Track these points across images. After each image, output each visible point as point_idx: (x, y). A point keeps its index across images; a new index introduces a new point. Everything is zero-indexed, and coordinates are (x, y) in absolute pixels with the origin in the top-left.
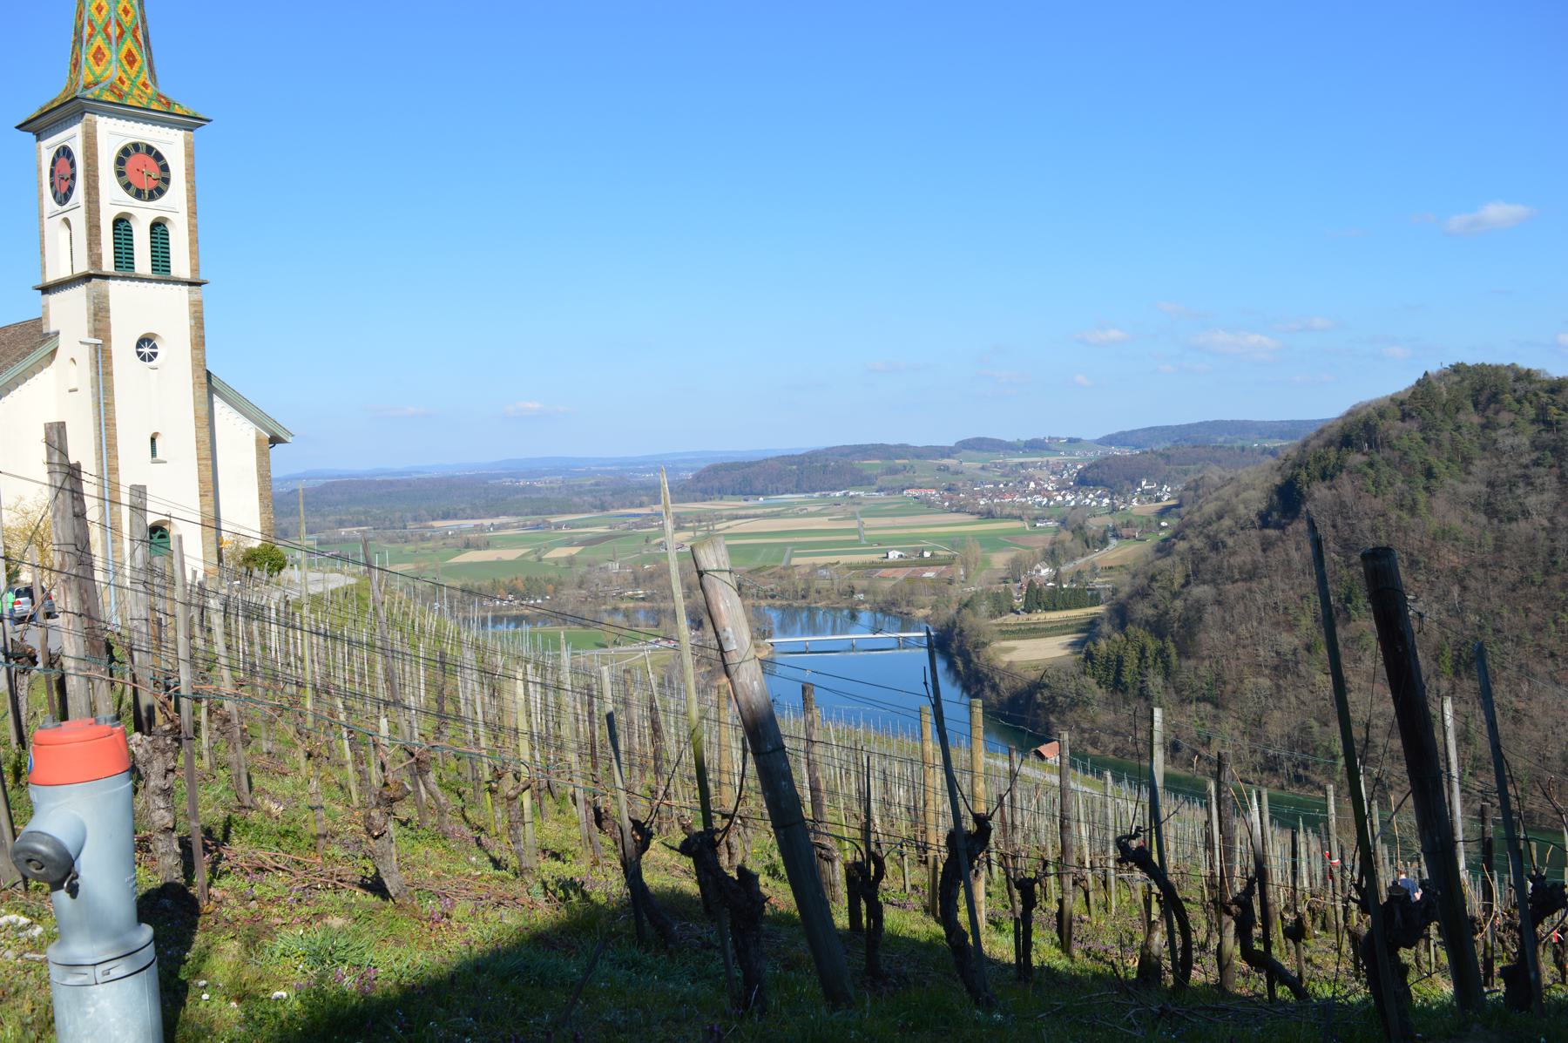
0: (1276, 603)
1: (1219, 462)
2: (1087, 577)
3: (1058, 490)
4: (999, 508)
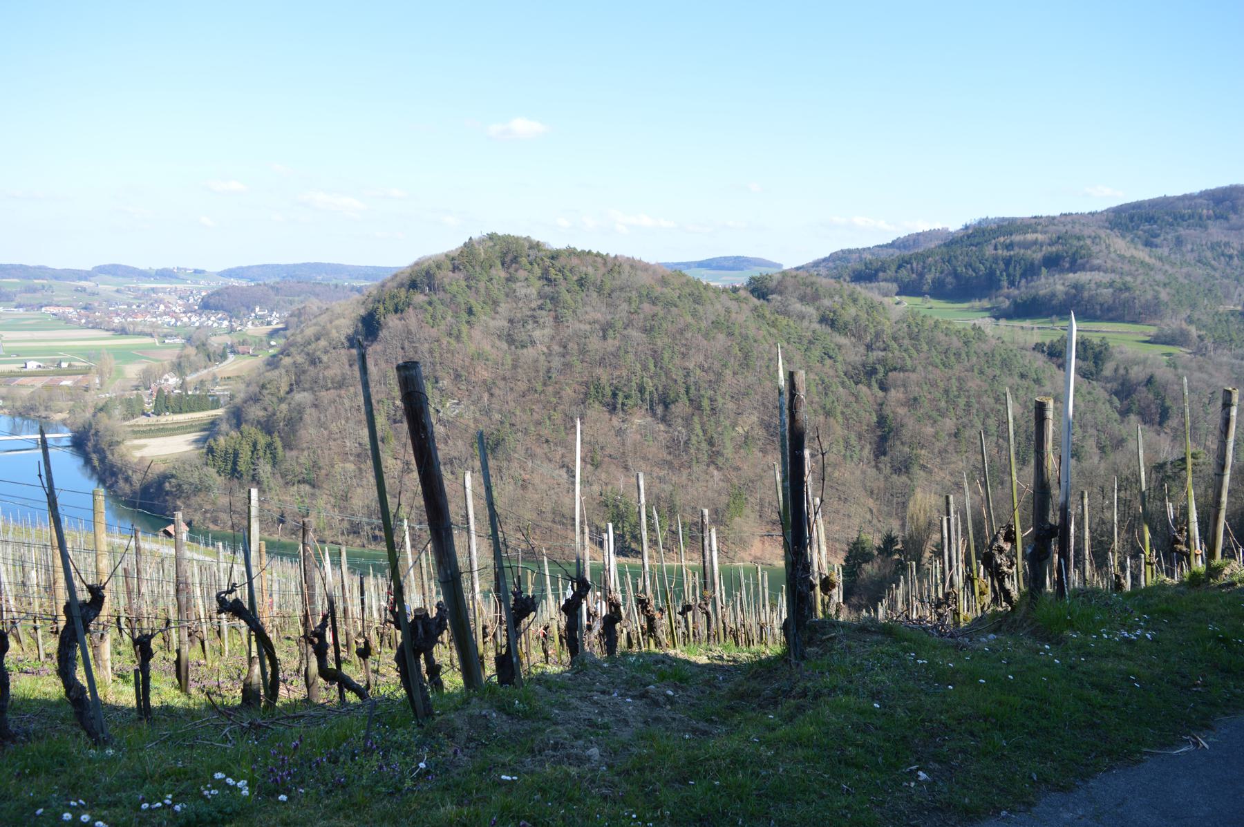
3: (184, 312)
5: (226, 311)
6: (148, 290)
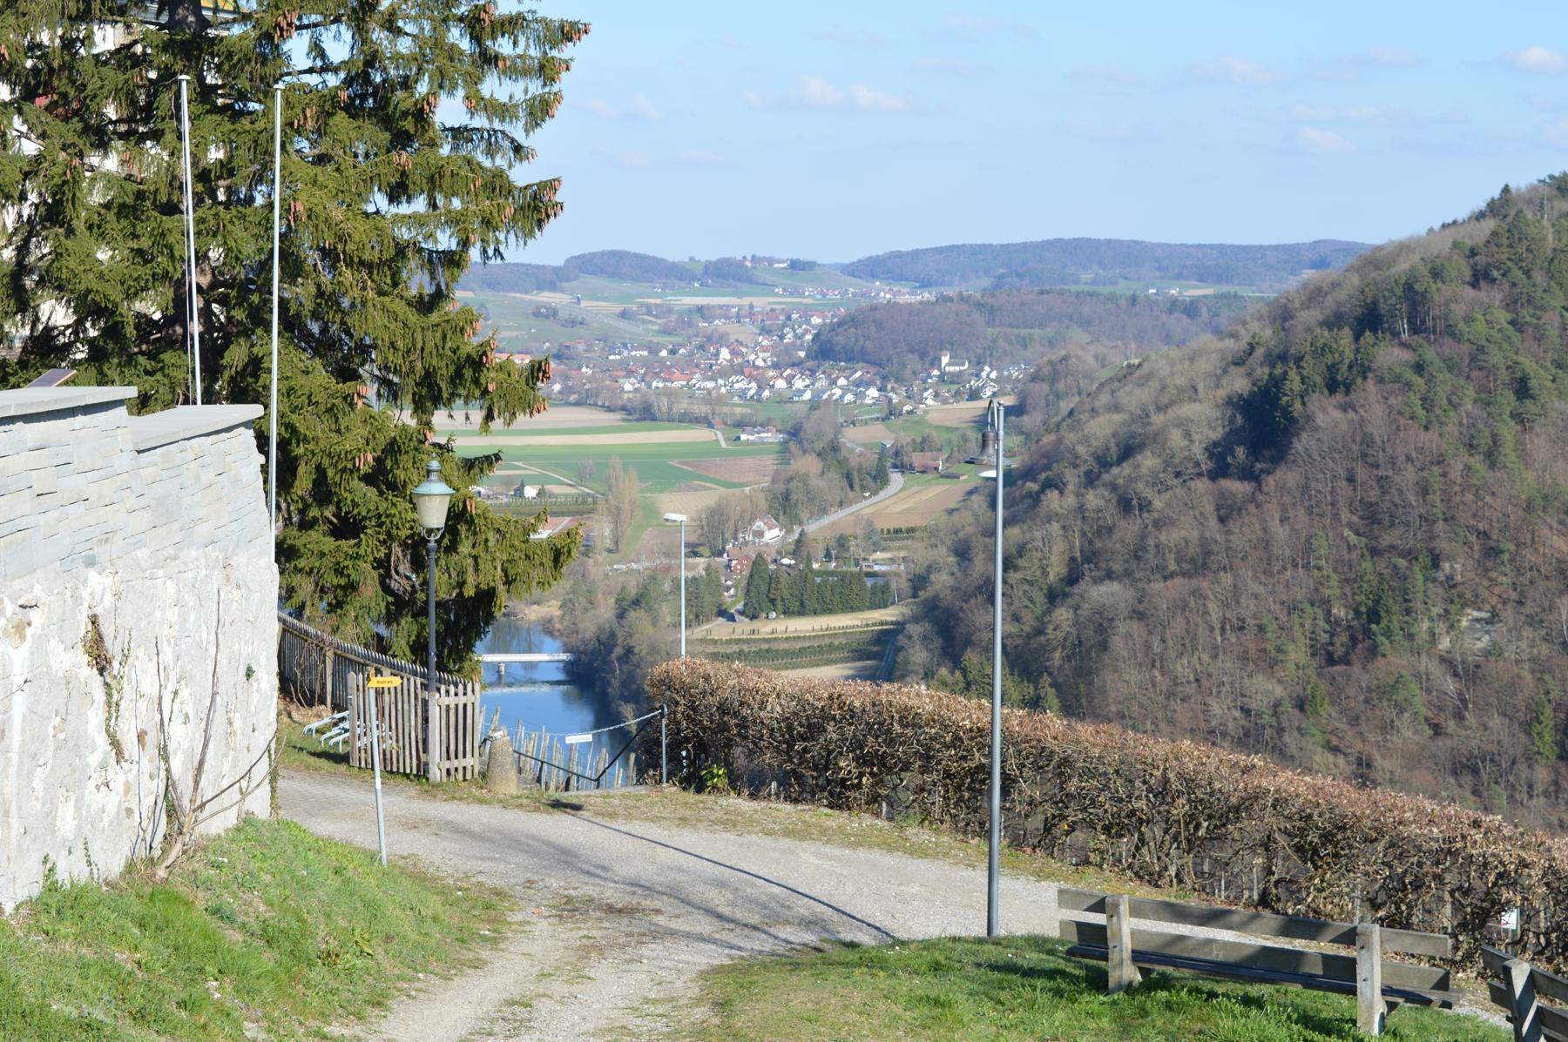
0: (1243, 620)
1: (1089, 323)
2: (854, 549)
3: (775, 366)
4: (665, 401)
5: (873, 363)
6: (690, 311)
